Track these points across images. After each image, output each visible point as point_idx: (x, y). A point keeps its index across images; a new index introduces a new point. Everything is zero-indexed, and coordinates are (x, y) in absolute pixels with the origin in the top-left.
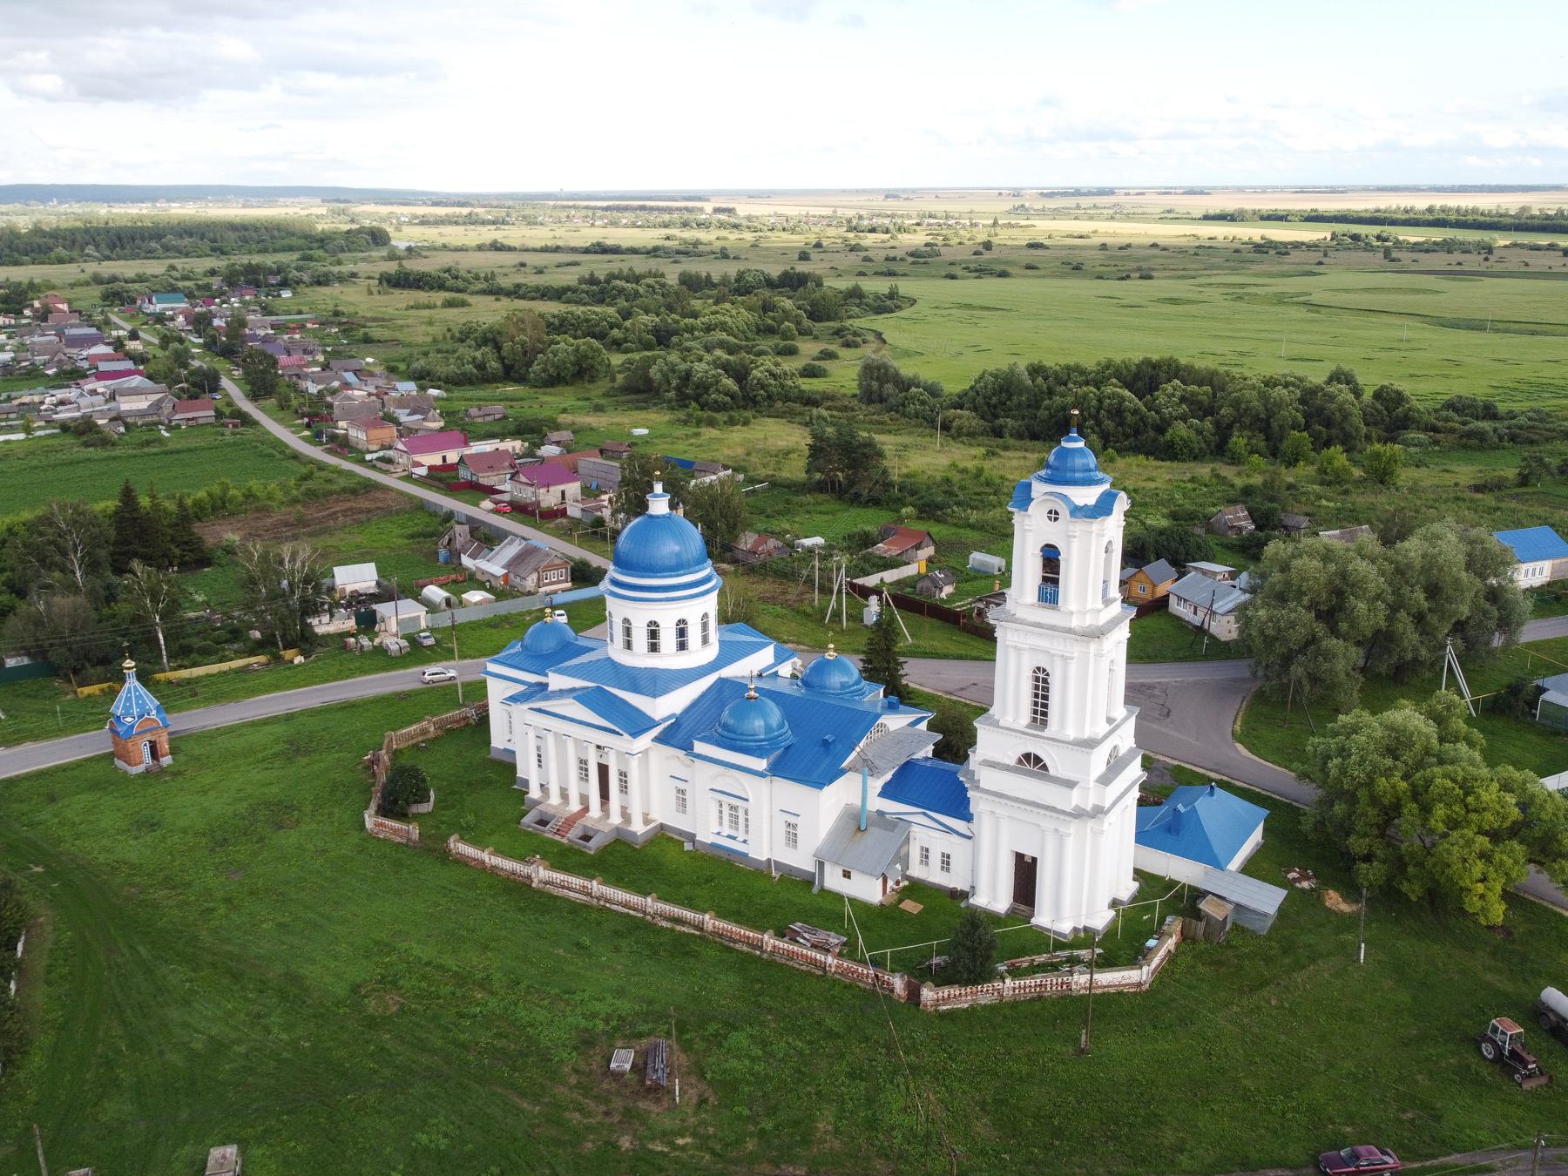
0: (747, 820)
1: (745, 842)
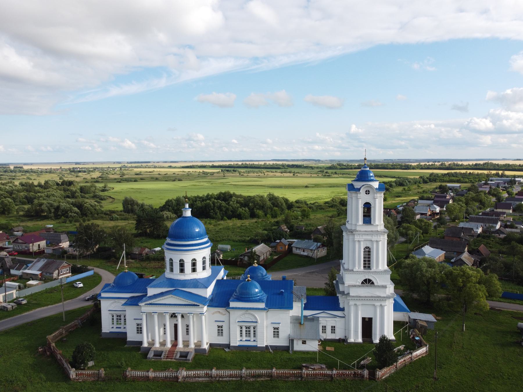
0: (125, 319)
1: (254, 341)
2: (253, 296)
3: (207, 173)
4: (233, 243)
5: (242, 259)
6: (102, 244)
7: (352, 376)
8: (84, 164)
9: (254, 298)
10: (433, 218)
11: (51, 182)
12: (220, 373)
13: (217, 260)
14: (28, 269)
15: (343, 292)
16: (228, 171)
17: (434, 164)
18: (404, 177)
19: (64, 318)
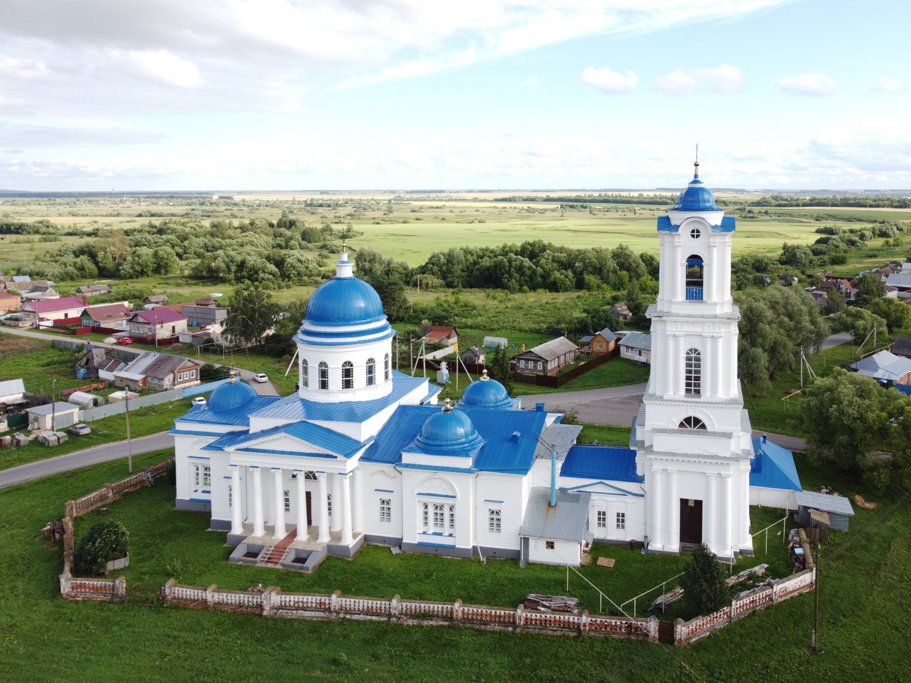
1: (451, 535)
2: (449, 443)
3: (534, 210)
5: (515, 365)
7: (623, 630)
9: (450, 448)
11: (260, 220)
14: (126, 371)
15: (643, 442)
16: (571, 207)
19: (130, 466)
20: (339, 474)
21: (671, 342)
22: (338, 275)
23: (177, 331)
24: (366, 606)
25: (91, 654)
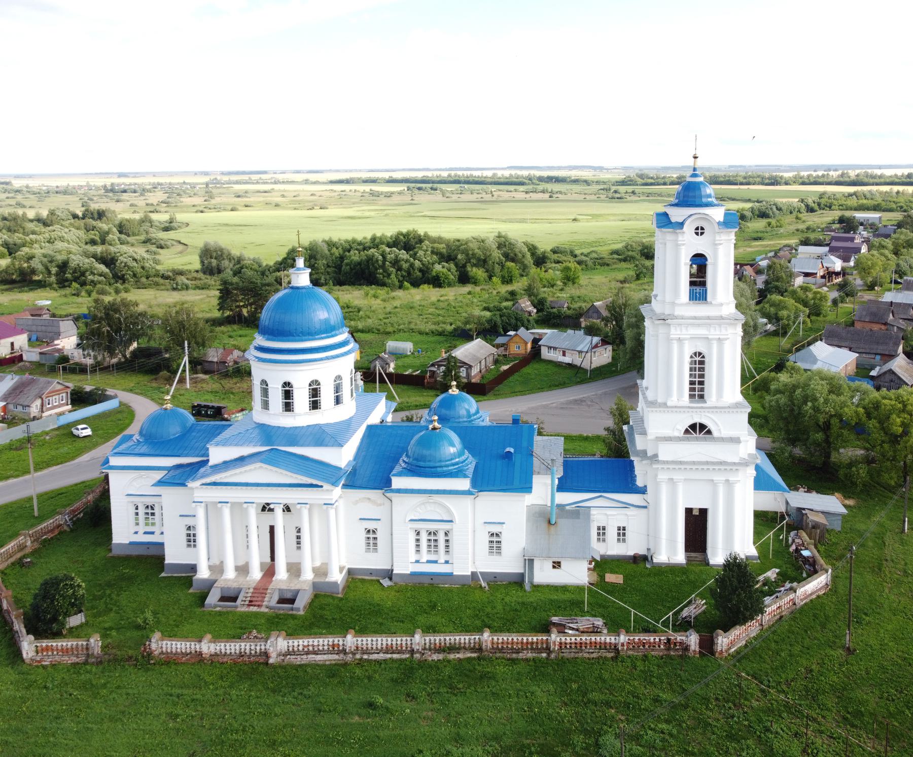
2: (443, 464)
4: (419, 337)
6: (144, 342)
7: (662, 647)
8: (135, 177)
9: (445, 469)
10: (829, 281)
12: (364, 643)
13: (380, 374)
16: (419, 189)
17: (828, 174)
18: (768, 200)
20: (325, 504)
21: (675, 346)
22: (294, 284)
23: (16, 347)
24: (384, 643)
25: (89, 723)
